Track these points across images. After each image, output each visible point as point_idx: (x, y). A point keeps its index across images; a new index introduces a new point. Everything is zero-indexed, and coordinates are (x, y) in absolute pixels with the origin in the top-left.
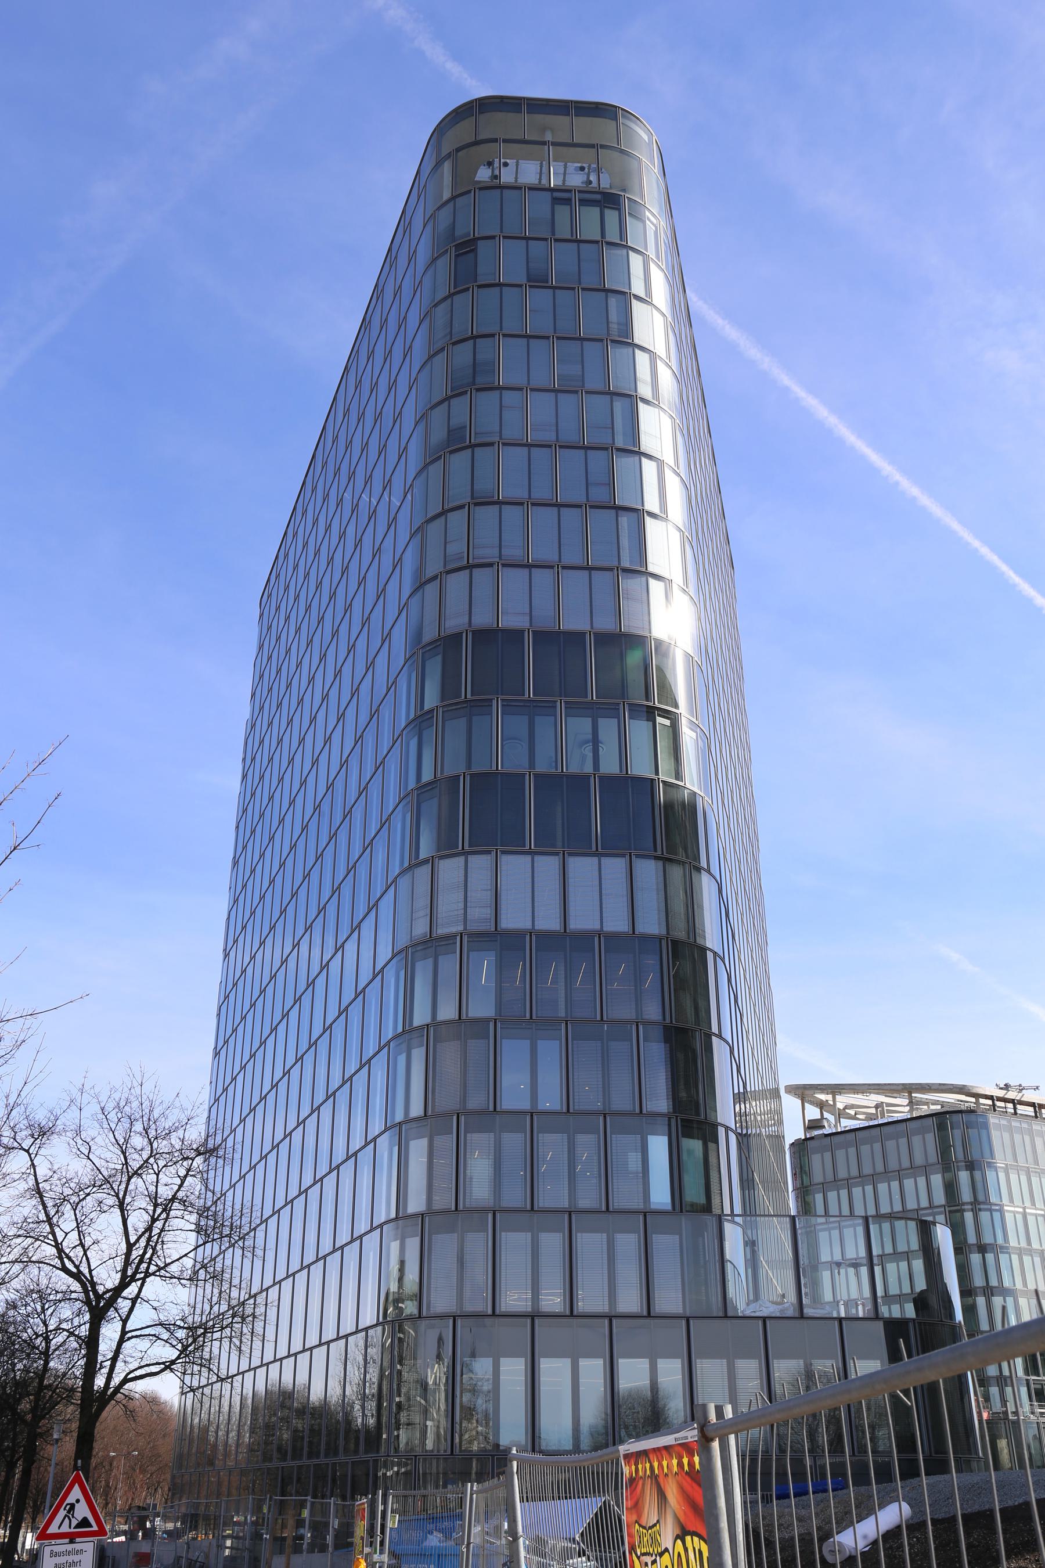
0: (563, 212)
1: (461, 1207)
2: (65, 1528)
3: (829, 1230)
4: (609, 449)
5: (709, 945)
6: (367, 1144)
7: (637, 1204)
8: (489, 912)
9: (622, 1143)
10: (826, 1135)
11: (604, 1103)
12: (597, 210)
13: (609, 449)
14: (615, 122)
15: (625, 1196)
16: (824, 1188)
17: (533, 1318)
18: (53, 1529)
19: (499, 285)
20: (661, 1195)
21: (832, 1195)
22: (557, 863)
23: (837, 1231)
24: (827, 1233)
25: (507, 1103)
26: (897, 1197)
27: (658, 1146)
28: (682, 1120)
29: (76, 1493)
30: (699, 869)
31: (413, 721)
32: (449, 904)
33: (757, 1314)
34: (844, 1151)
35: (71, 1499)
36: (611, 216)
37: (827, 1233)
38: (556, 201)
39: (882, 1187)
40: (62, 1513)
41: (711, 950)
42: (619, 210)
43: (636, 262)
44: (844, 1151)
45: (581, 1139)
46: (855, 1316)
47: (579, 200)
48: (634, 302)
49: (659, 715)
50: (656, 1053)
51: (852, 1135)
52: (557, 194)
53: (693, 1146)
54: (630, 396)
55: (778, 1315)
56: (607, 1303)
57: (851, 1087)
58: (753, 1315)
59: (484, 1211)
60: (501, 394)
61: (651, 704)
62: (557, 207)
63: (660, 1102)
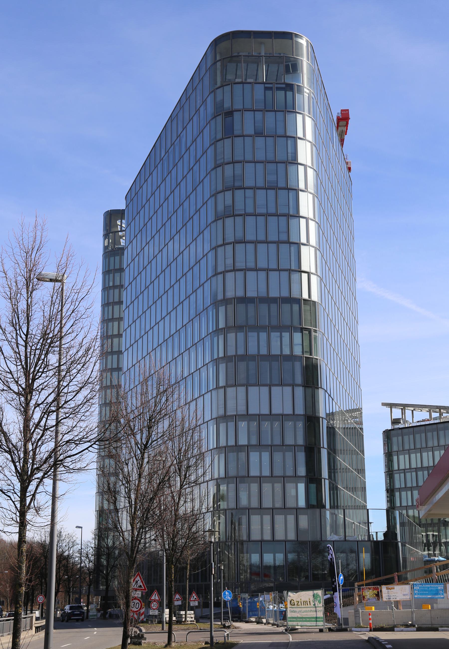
0: (269, 93)
1: (238, 508)
2: (193, 599)
3: (400, 473)
4: (288, 216)
5: (321, 416)
6: (145, 333)
7: (294, 505)
8: (244, 408)
9: (290, 487)
10: (400, 429)
11: (284, 474)
12: (284, 92)
13: (288, 216)
14: (292, 40)
15: (290, 504)
16: (398, 453)
17: (261, 542)
18: (191, 600)
19: (243, 136)
20: (302, 503)
21: (401, 457)
22: (268, 389)
23: (403, 474)
24: (398, 474)
25: (252, 474)
26: (431, 459)
27: (302, 487)
28: (309, 478)
29: (194, 594)
30: (318, 388)
31: (212, 304)
32: (231, 404)
33: (331, 540)
34: (408, 436)
35: (193, 595)
36: (289, 94)
37: (398, 474)
38: (266, 89)
39: (425, 455)
40: (192, 597)
41: (321, 417)
42: (293, 92)
43: (299, 118)
44: (408, 436)
45: (276, 485)
46: (364, 540)
47: (276, 88)
48: (298, 140)
49: (304, 330)
50: (301, 457)
51: (412, 429)
52: (266, 85)
53: (313, 487)
54: (296, 190)
55: (339, 540)
56: (284, 537)
57: (413, 406)
58: (330, 540)
59: (245, 509)
60: (244, 138)
61: (301, 327)
62: (266, 91)
63: (302, 471)
